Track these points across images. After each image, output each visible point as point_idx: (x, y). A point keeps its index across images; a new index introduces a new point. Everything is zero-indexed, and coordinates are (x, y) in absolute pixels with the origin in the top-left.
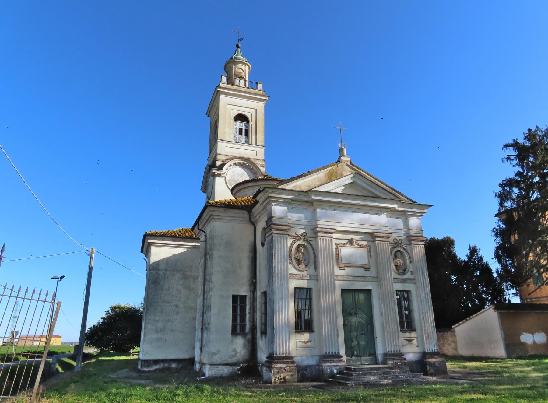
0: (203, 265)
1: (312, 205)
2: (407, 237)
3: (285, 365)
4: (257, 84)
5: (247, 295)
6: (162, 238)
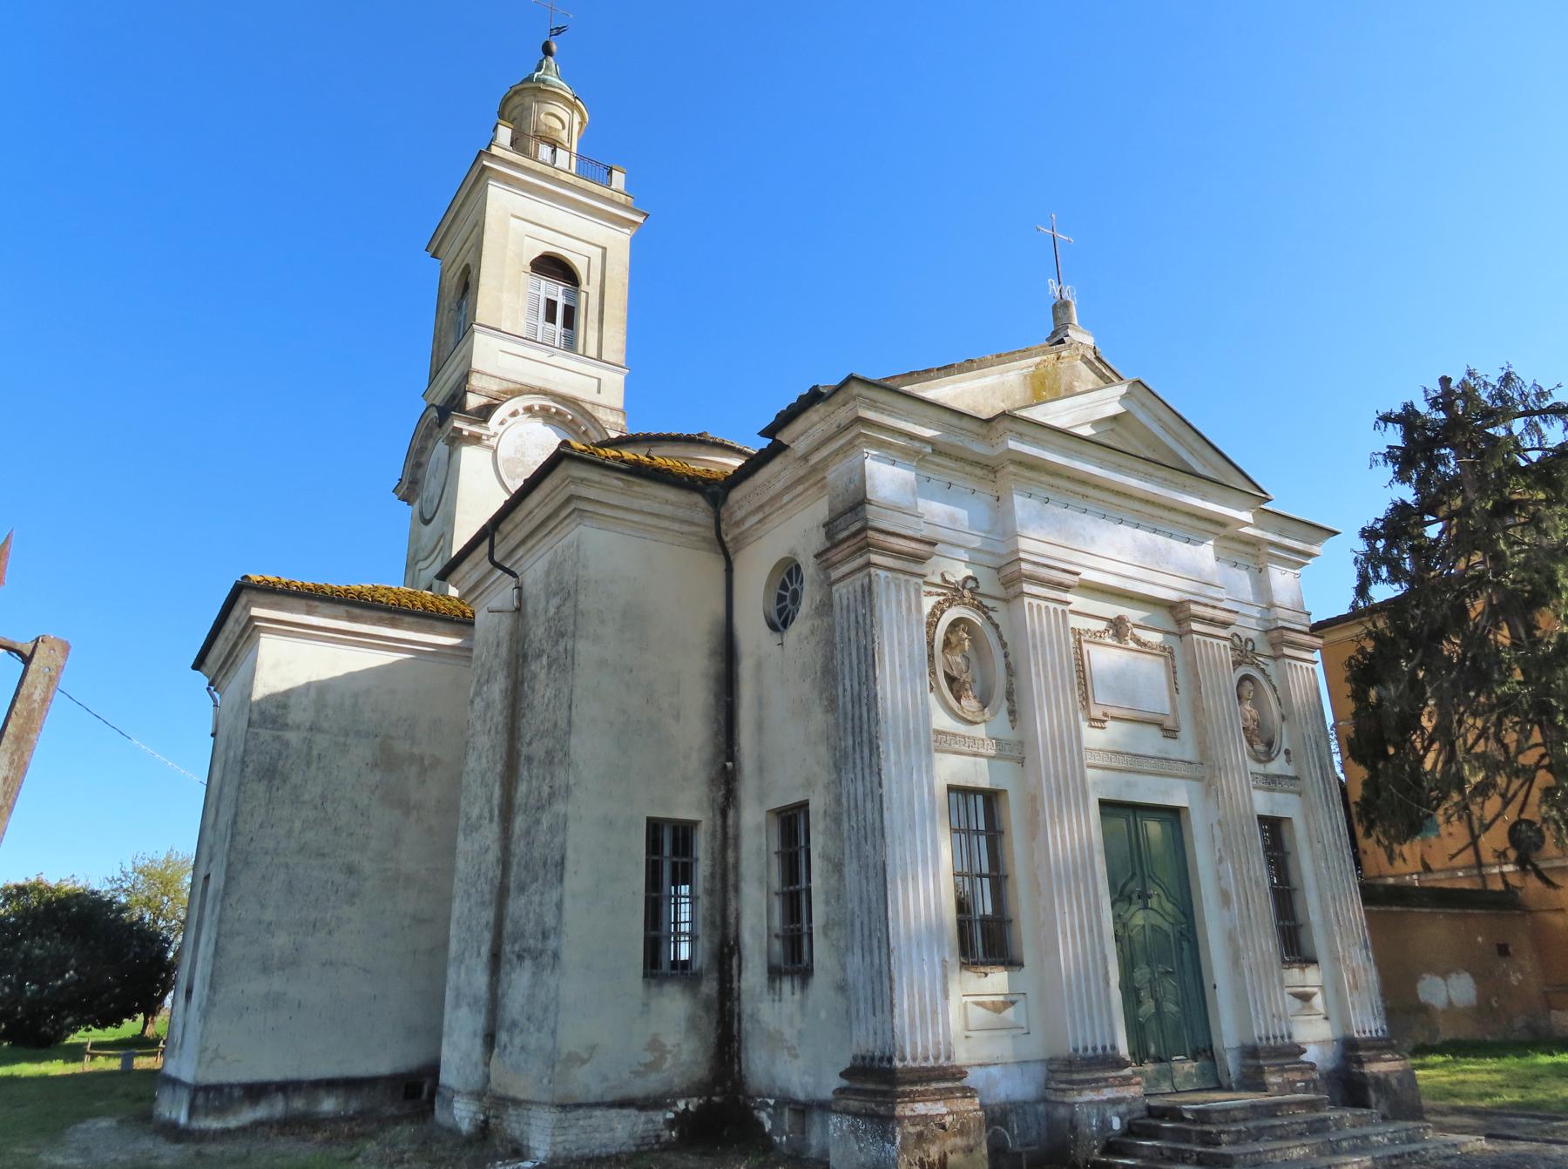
1: (991, 476)
2: (1266, 632)
3: (941, 1104)
4: (610, 173)
6: (308, 606)
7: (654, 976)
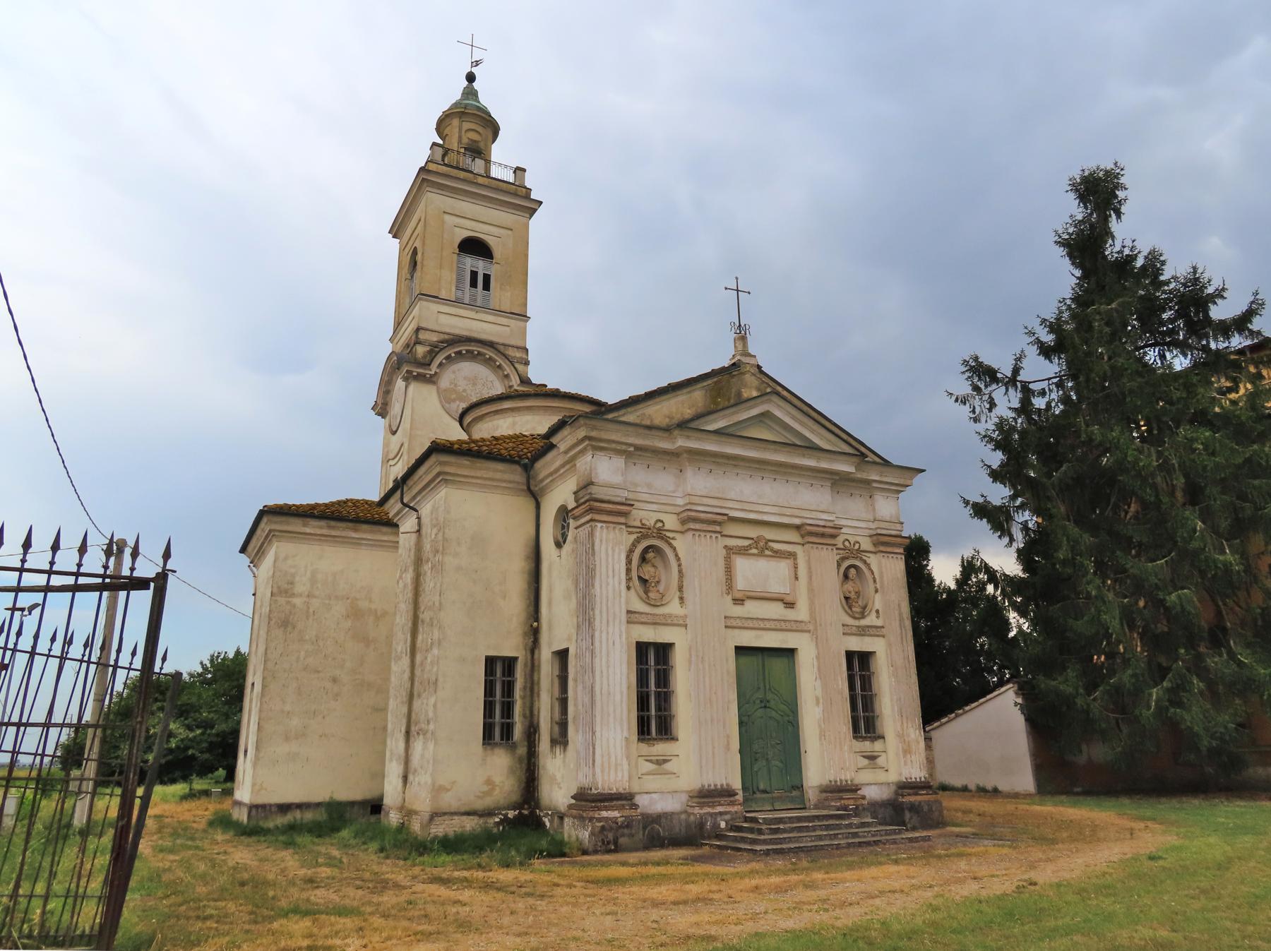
0: (410, 587)
5: (516, 658)
7: (489, 744)
